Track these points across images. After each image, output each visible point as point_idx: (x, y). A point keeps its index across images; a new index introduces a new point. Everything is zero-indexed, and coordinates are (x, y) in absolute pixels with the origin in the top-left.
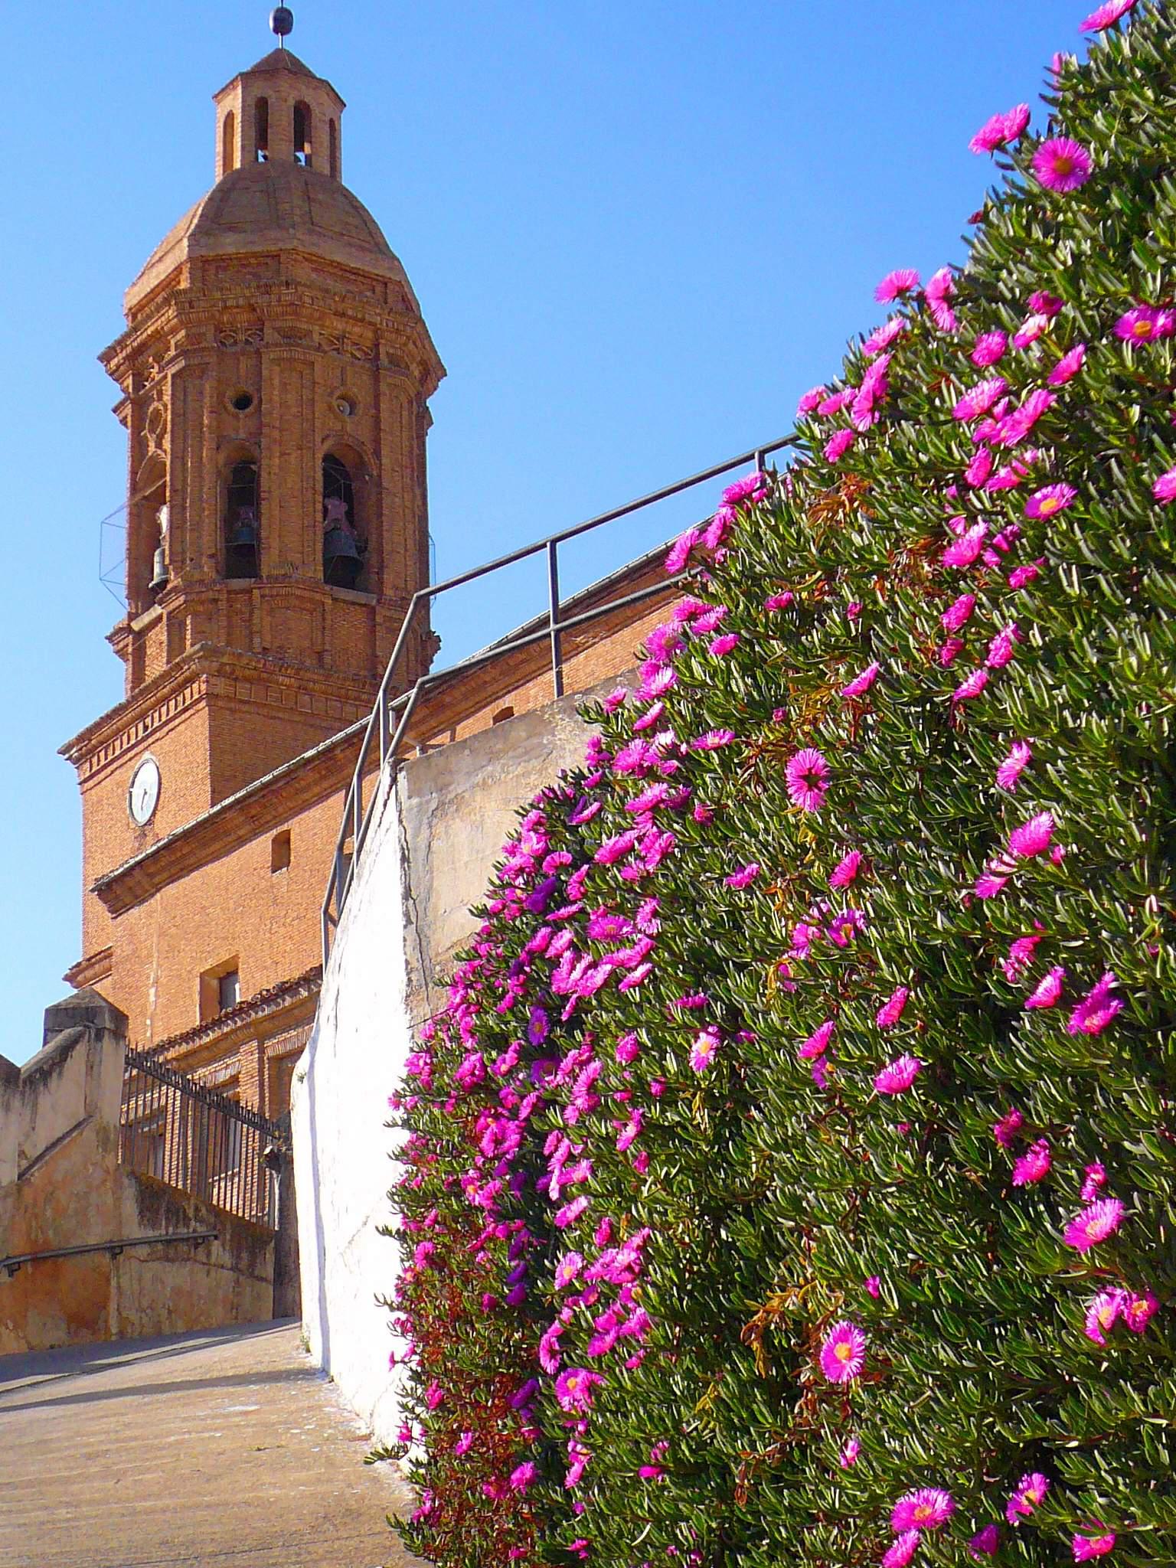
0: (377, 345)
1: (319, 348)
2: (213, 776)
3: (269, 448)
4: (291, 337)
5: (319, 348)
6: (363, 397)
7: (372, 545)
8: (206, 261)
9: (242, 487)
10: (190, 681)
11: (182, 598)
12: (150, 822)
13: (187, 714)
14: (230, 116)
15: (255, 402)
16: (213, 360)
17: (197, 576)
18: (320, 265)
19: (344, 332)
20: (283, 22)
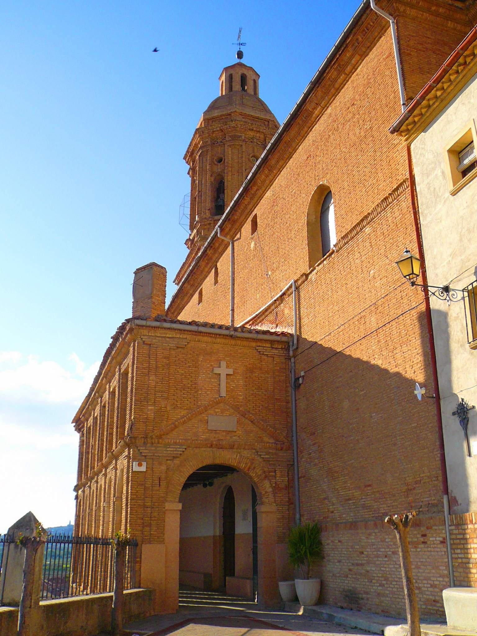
0: (265, 140)
1: (244, 141)
3: (227, 173)
4: (235, 138)
5: (244, 141)
8: (209, 120)
14: (223, 82)
16: (210, 148)
17: (204, 216)
18: (245, 116)
20: (240, 55)
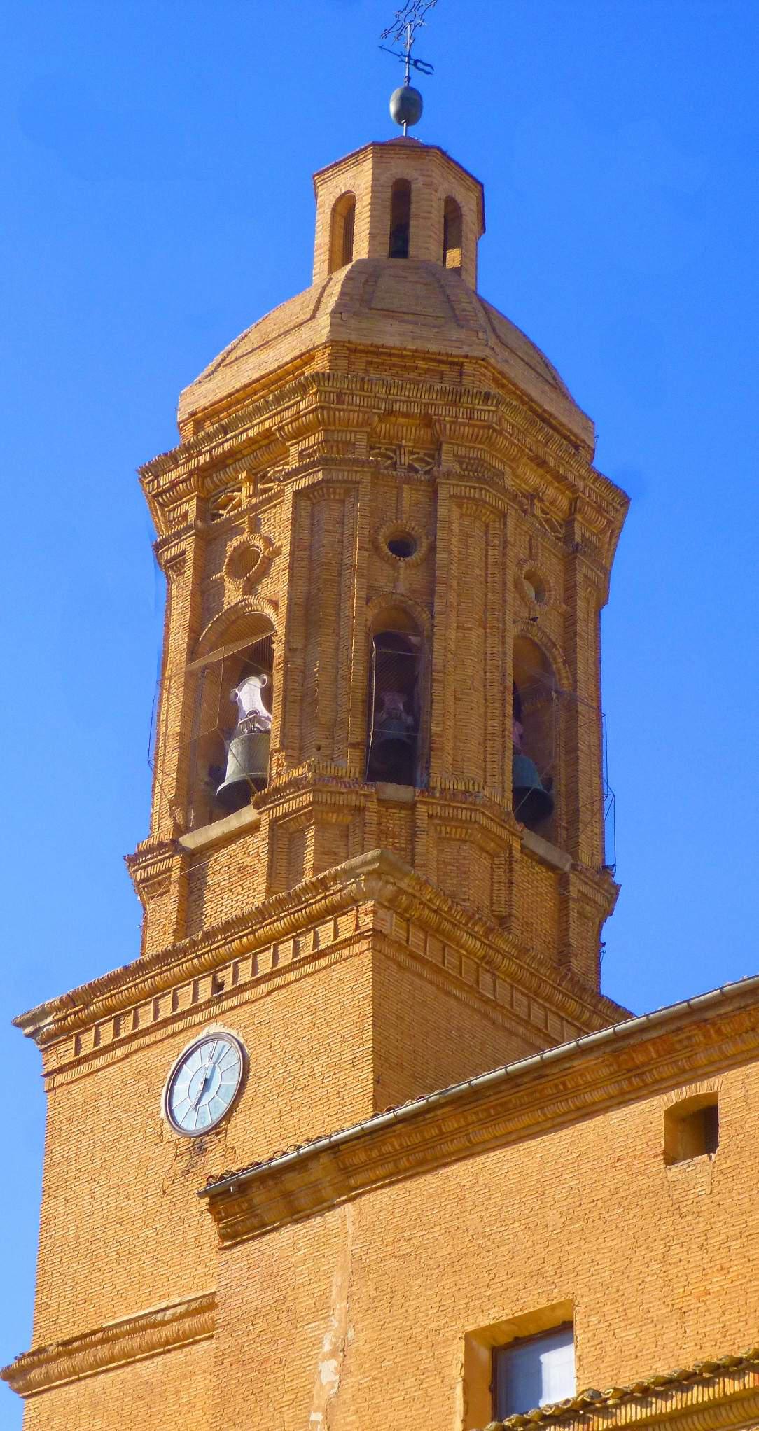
0: (569, 523)
2: (381, 1057)
4: (475, 471)
6: (554, 580)
7: (560, 786)
9: (400, 661)
10: (336, 910)
11: (307, 798)
12: (216, 1129)
13: (320, 963)
15: (417, 556)
19: (535, 490)
20: (410, 107)
